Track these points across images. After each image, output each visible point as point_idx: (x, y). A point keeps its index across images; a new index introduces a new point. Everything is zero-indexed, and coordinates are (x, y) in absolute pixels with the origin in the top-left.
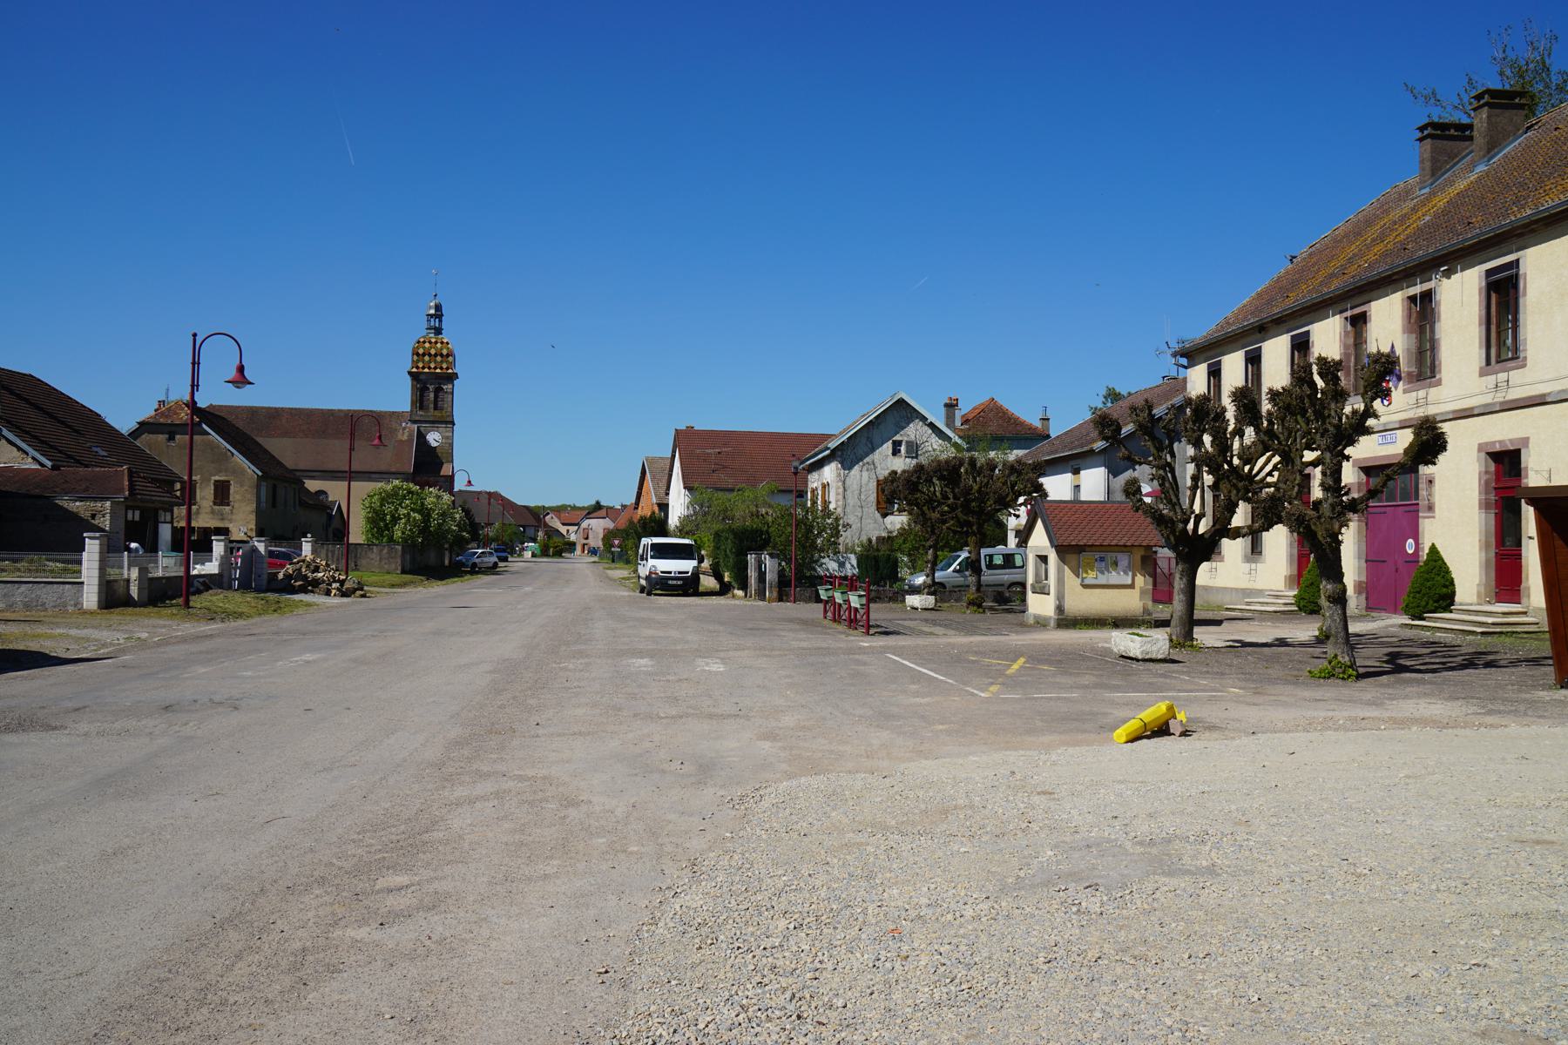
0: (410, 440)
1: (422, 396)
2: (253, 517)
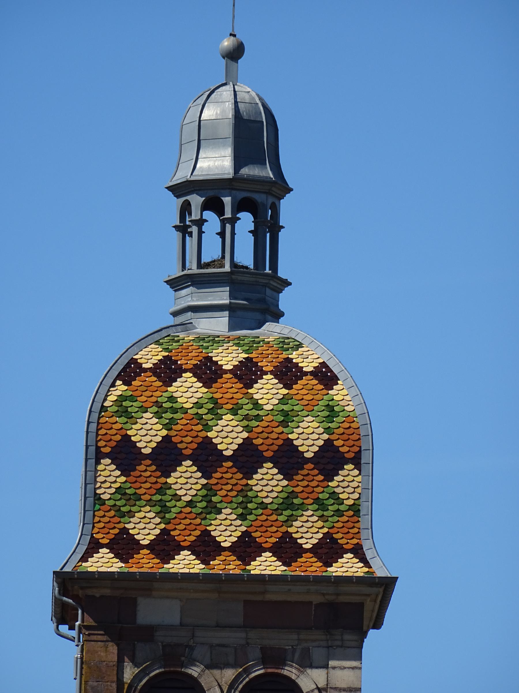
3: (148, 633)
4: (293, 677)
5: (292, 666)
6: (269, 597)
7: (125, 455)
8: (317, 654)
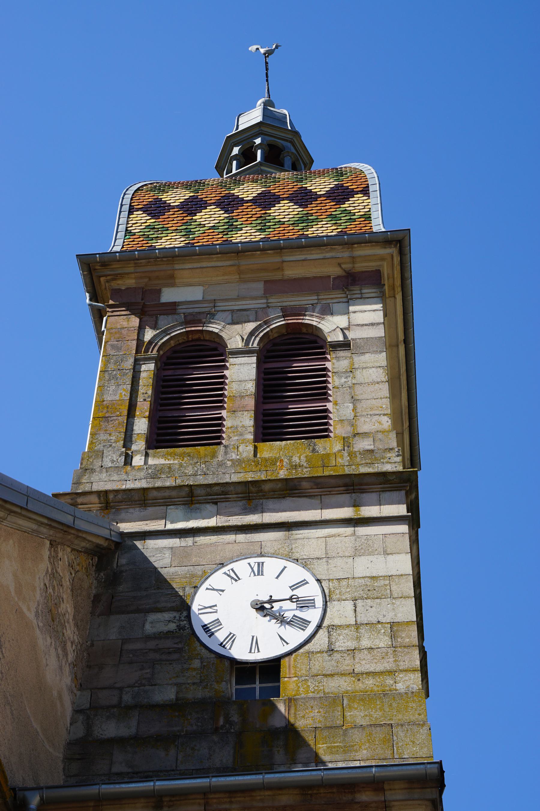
3: (172, 308)
4: (314, 323)
5: (312, 316)
7: (157, 209)
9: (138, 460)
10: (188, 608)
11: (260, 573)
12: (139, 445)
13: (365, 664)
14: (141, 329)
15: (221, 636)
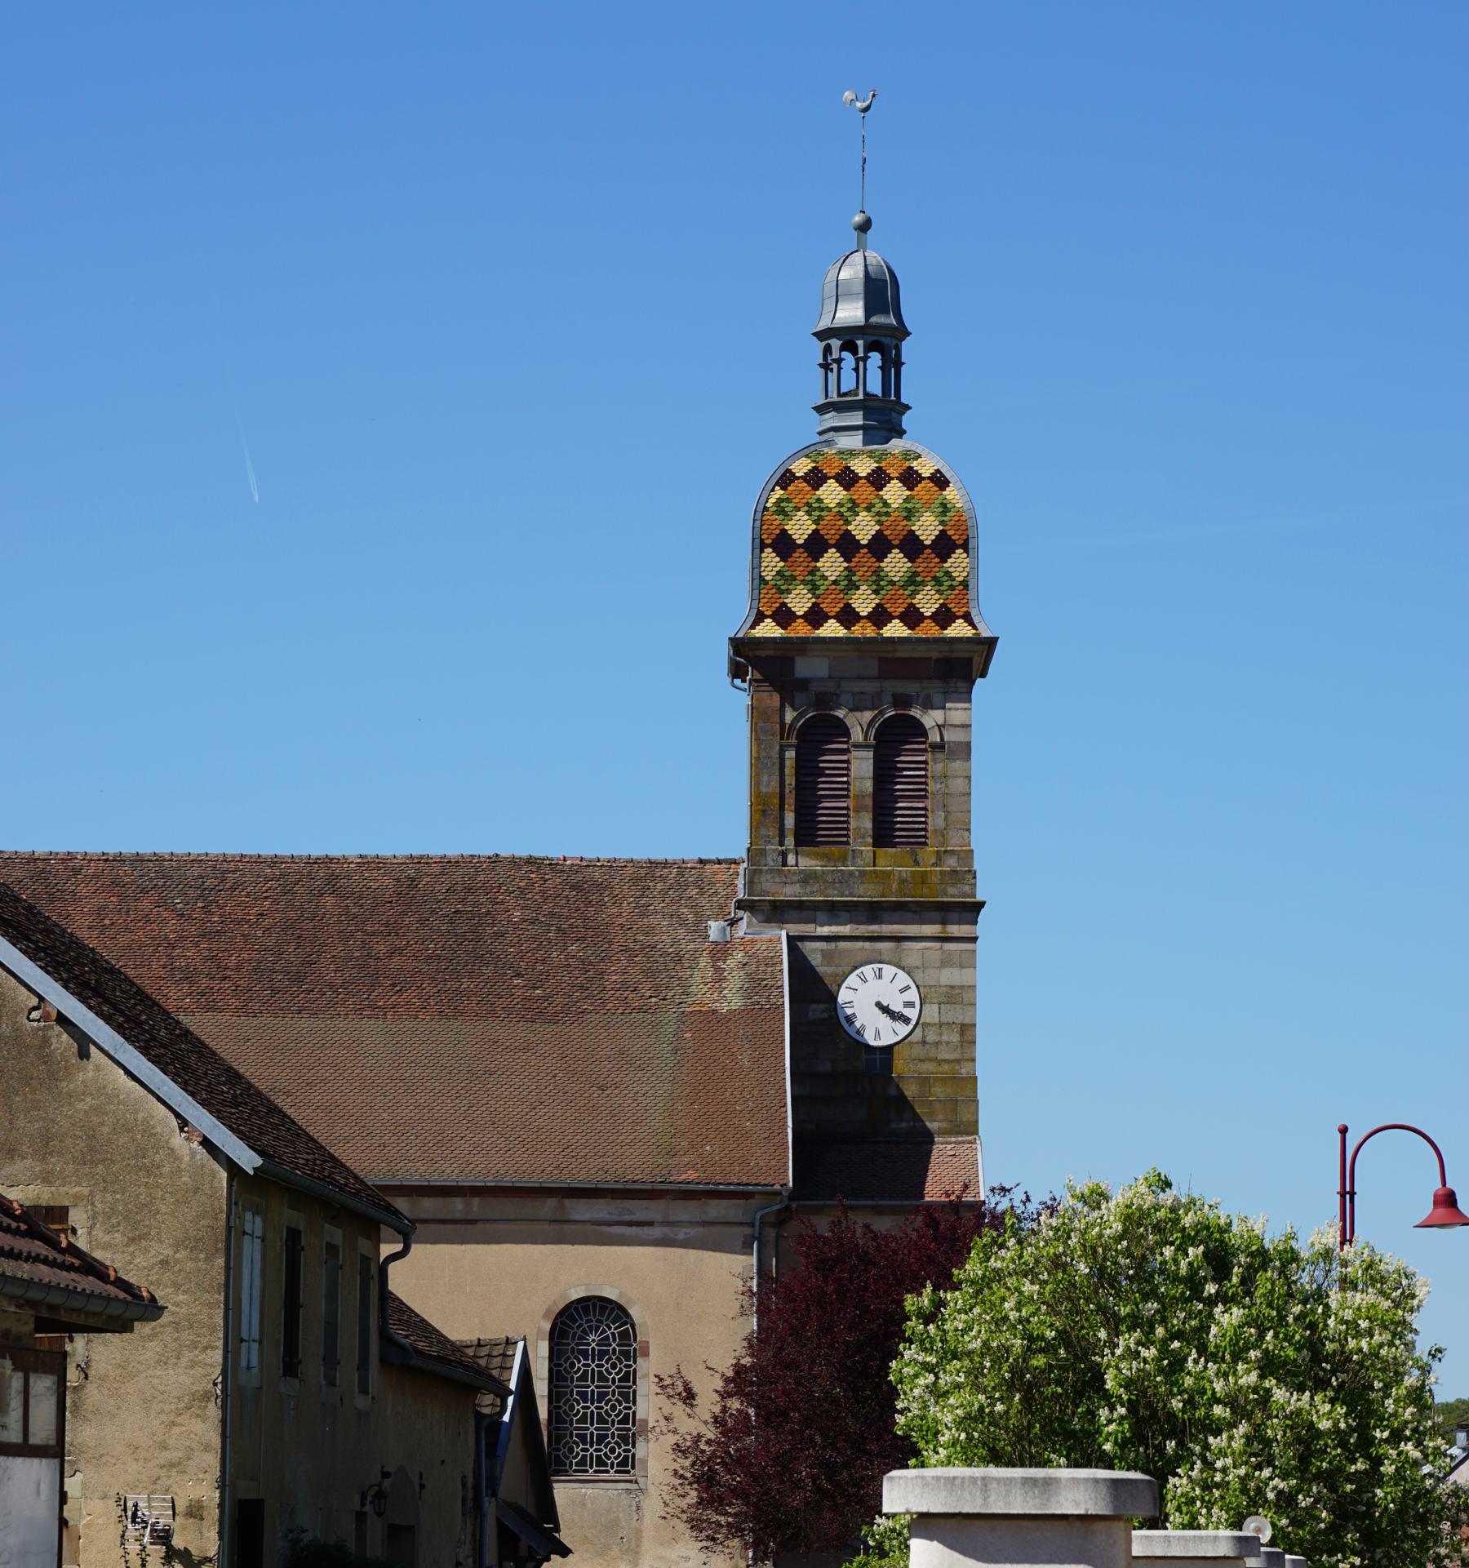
0: (759, 1013)
1: (808, 771)
2: (206, 1429)
3: (804, 684)
6: (898, 655)
7: (783, 545)
8: (937, 698)
9: (791, 859)
10: (835, 999)
11: (880, 977)
12: (790, 841)
13: (943, 1055)
14: (782, 707)
15: (858, 1024)
